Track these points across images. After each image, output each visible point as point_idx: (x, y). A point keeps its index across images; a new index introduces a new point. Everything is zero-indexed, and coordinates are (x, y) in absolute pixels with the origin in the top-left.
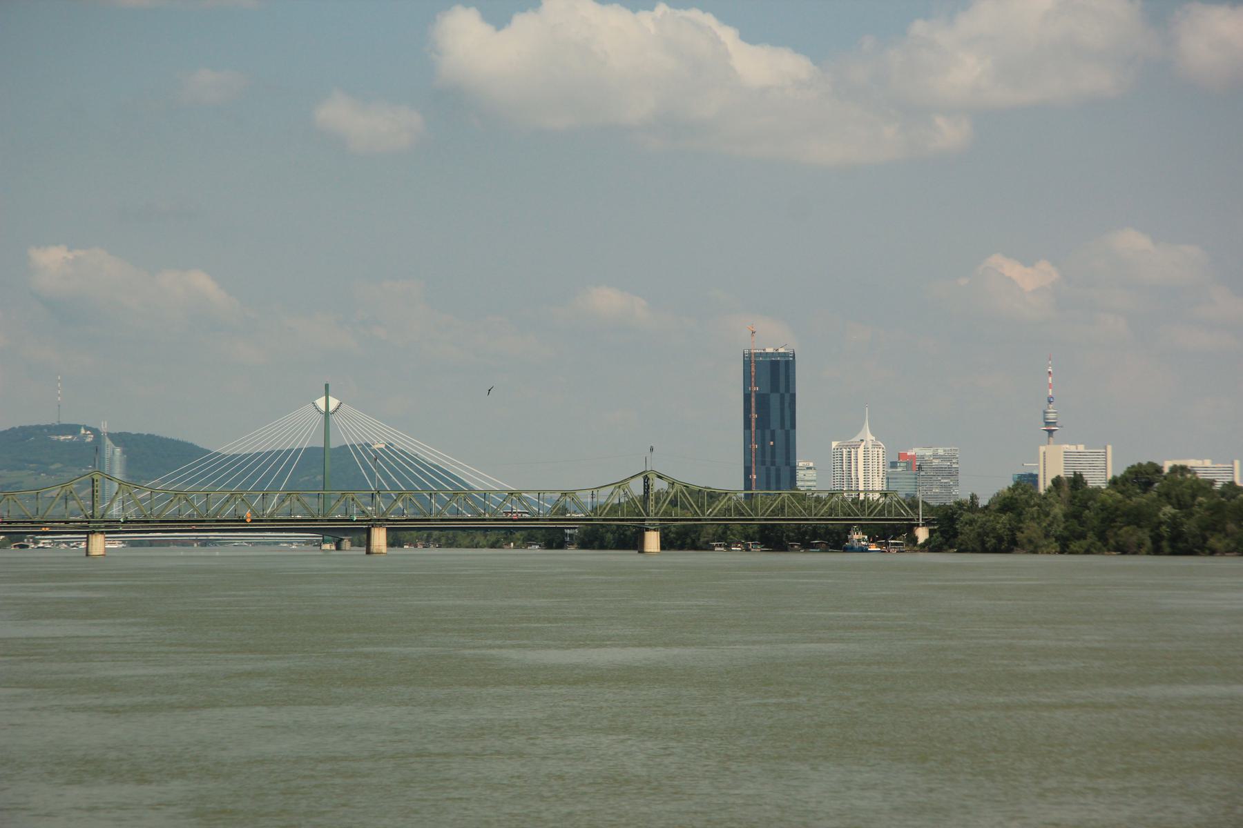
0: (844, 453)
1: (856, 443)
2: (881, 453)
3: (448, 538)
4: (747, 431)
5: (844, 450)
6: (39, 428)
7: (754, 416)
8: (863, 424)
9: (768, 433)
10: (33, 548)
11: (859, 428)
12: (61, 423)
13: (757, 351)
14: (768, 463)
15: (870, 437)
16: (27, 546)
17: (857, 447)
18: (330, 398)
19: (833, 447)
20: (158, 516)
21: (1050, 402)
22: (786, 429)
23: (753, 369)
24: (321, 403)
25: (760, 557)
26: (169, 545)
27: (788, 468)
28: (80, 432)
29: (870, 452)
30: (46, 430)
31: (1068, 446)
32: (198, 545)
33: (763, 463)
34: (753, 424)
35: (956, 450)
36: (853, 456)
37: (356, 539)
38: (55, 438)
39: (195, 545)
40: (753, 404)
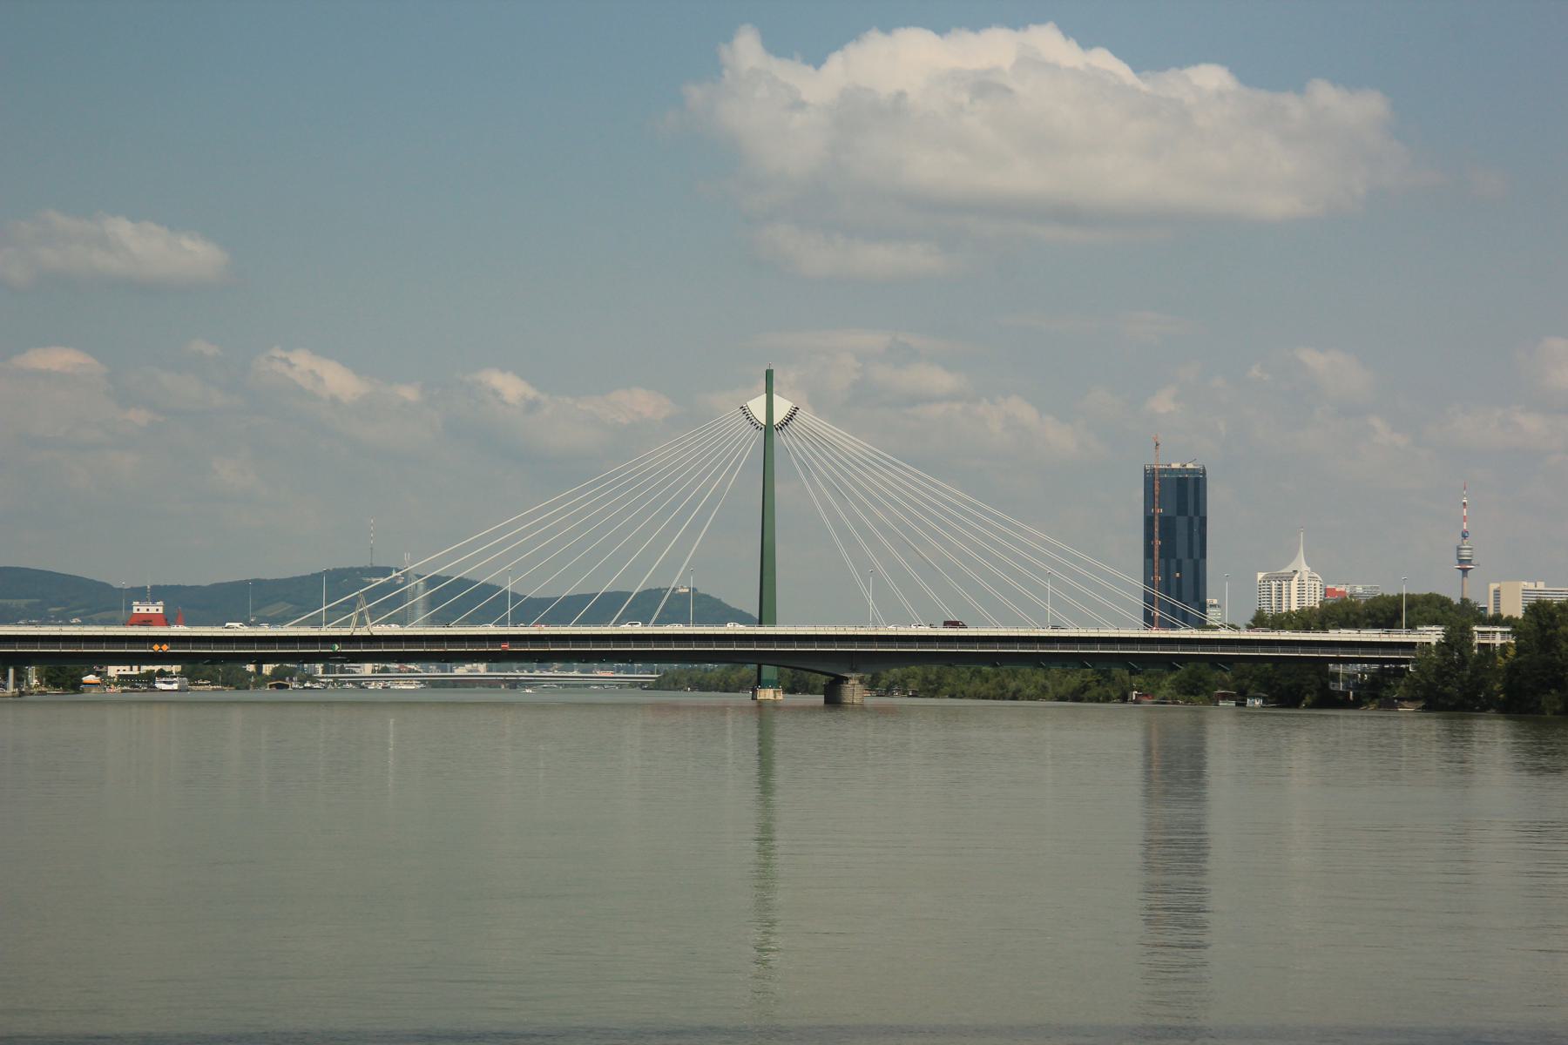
0: (1273, 587)
2: (1318, 586)
3: (926, 680)
4: (1151, 560)
6: (352, 570)
7: (1158, 543)
8: (1298, 549)
10: (294, 689)
11: (1292, 557)
12: (374, 565)
13: (1161, 467)
15: (1304, 569)
17: (1290, 579)
18: (776, 397)
21: (1465, 537)
22: (1175, 560)
23: (1157, 488)
24: (757, 407)
29: (1306, 586)
30: (358, 573)
31: (1526, 583)
34: (1157, 553)
36: (1284, 590)
37: (507, 684)
39: (503, 687)
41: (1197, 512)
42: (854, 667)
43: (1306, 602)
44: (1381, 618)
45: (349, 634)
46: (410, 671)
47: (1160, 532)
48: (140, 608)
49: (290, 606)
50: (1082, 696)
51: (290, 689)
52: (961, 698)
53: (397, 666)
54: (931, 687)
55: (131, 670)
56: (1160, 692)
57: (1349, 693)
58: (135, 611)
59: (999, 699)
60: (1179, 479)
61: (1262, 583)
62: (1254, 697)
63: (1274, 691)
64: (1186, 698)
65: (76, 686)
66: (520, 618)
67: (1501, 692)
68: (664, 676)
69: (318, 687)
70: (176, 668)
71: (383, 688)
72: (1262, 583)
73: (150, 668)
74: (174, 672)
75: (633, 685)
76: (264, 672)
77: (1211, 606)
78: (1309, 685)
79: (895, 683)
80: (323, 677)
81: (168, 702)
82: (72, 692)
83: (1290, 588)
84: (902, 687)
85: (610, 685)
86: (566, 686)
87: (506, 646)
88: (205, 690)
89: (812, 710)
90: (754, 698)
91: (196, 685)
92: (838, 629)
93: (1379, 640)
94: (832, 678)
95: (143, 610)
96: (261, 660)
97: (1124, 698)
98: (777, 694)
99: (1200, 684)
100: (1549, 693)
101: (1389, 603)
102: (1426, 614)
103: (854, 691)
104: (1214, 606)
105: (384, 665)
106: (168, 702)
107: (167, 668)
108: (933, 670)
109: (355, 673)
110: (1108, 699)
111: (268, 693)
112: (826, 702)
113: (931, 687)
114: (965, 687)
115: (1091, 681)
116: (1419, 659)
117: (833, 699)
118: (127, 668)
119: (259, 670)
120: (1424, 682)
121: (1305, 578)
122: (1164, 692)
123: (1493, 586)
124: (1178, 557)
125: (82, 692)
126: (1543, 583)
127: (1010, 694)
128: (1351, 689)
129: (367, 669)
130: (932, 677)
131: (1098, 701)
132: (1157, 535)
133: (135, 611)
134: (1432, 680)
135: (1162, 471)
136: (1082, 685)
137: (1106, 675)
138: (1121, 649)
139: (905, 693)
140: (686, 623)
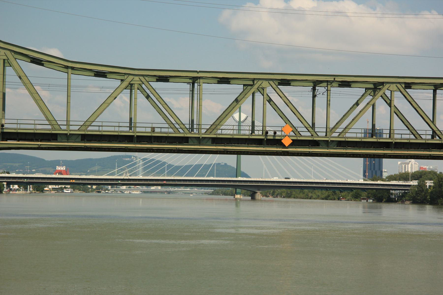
0: (403, 166)
1: (408, 163)
2: (417, 166)
5: (403, 165)
10: (103, 193)
16: (101, 192)
17: (408, 164)
19: (399, 164)
20: (88, 123)
26: (157, 193)
27: (380, 171)
28: (132, 157)
29: (413, 166)
30: (121, 157)
32: (167, 193)
33: (371, 169)
35: (437, 167)
36: (406, 167)
37: (167, 193)
38: (124, 159)
39: (166, 193)
42: (259, 189)
43: (413, 170)
44: (416, 177)
45: (123, 178)
46: (137, 188)
48: (58, 168)
49: (100, 167)
50: (328, 198)
51: (102, 193)
52: (296, 198)
53: (133, 186)
54: (289, 195)
55: (56, 186)
56: (348, 197)
57: (396, 199)
58: (57, 169)
59: (306, 199)
61: (400, 165)
62: (370, 199)
63: (376, 198)
64: (354, 199)
65: (42, 191)
66: (169, 174)
67: (429, 199)
68: (214, 191)
69: (110, 192)
70: (68, 186)
71: (129, 193)
72: (400, 165)
73: (61, 186)
74: (68, 187)
75: (206, 193)
76: (93, 187)
77: (385, 172)
78: (385, 196)
79: (279, 194)
80: (111, 189)
81: (67, 195)
82: (42, 192)
83: (408, 167)
84: (281, 195)
85: (199, 193)
86: (185, 193)
87: (165, 182)
88: (77, 192)
89: (248, 200)
90: (234, 197)
91: (75, 191)
92: (255, 179)
93: (402, 184)
94: (253, 192)
95: (59, 169)
96: (92, 184)
97: (339, 199)
98: (241, 196)
99: (358, 195)
100: (440, 199)
101: (419, 173)
102: (428, 176)
103: (259, 196)
104: (385, 172)
105: (129, 186)
106: (67, 195)
107: (66, 186)
108: (289, 191)
109: (120, 188)
110: (334, 199)
111: (95, 193)
112: (251, 199)
113: (289, 195)
114: (298, 195)
115: (331, 194)
116: (411, 190)
117: (253, 197)
118: (55, 186)
119: (92, 188)
120: (412, 196)
121: (413, 163)
122: (349, 198)
125: (44, 192)
127: (309, 198)
128: (396, 197)
129: (124, 187)
130: (289, 192)
131: (332, 200)
133: (57, 169)
134: (415, 195)
136: (328, 195)
137: (334, 192)
138: (348, 186)
139: (281, 197)
140: (214, 176)
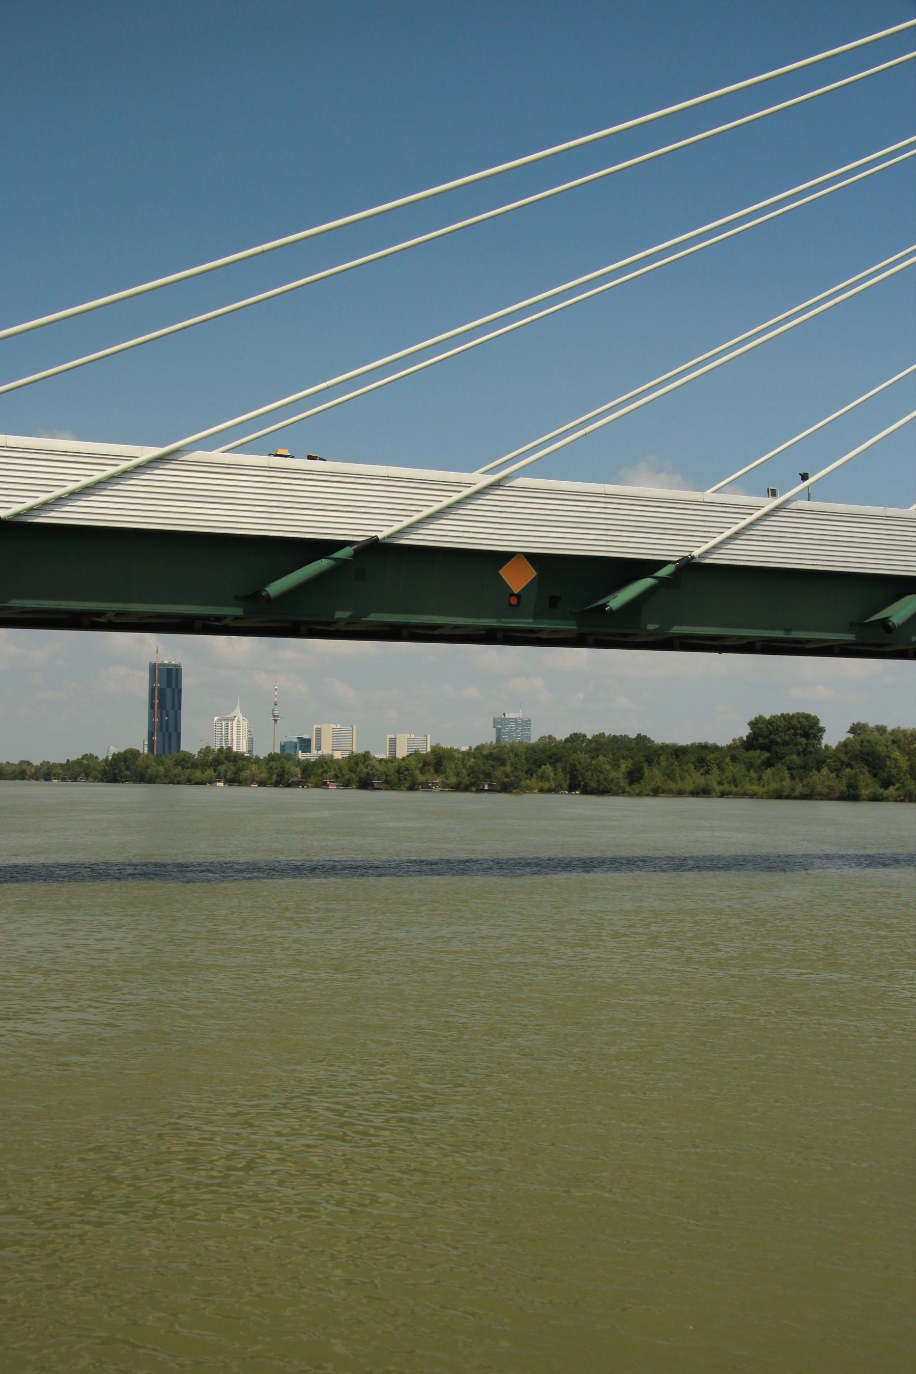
0: (223, 724)
4: (153, 710)
5: (223, 722)
9: (164, 711)
11: (232, 709)
14: (167, 733)
15: (240, 715)
17: (233, 720)
25: (355, 795)
29: (241, 724)
34: (156, 707)
38: (363, 619)
40: (156, 695)
41: (177, 687)
47: (158, 696)
60: (168, 668)
72: (217, 722)
123: (315, 726)
124: (168, 709)
126: (339, 725)
132: (156, 698)
135: (160, 665)
